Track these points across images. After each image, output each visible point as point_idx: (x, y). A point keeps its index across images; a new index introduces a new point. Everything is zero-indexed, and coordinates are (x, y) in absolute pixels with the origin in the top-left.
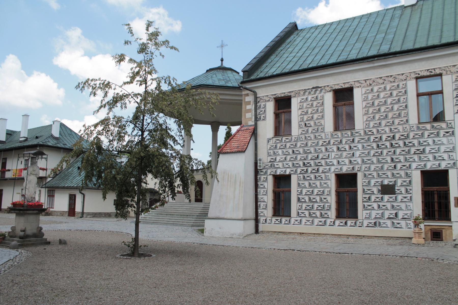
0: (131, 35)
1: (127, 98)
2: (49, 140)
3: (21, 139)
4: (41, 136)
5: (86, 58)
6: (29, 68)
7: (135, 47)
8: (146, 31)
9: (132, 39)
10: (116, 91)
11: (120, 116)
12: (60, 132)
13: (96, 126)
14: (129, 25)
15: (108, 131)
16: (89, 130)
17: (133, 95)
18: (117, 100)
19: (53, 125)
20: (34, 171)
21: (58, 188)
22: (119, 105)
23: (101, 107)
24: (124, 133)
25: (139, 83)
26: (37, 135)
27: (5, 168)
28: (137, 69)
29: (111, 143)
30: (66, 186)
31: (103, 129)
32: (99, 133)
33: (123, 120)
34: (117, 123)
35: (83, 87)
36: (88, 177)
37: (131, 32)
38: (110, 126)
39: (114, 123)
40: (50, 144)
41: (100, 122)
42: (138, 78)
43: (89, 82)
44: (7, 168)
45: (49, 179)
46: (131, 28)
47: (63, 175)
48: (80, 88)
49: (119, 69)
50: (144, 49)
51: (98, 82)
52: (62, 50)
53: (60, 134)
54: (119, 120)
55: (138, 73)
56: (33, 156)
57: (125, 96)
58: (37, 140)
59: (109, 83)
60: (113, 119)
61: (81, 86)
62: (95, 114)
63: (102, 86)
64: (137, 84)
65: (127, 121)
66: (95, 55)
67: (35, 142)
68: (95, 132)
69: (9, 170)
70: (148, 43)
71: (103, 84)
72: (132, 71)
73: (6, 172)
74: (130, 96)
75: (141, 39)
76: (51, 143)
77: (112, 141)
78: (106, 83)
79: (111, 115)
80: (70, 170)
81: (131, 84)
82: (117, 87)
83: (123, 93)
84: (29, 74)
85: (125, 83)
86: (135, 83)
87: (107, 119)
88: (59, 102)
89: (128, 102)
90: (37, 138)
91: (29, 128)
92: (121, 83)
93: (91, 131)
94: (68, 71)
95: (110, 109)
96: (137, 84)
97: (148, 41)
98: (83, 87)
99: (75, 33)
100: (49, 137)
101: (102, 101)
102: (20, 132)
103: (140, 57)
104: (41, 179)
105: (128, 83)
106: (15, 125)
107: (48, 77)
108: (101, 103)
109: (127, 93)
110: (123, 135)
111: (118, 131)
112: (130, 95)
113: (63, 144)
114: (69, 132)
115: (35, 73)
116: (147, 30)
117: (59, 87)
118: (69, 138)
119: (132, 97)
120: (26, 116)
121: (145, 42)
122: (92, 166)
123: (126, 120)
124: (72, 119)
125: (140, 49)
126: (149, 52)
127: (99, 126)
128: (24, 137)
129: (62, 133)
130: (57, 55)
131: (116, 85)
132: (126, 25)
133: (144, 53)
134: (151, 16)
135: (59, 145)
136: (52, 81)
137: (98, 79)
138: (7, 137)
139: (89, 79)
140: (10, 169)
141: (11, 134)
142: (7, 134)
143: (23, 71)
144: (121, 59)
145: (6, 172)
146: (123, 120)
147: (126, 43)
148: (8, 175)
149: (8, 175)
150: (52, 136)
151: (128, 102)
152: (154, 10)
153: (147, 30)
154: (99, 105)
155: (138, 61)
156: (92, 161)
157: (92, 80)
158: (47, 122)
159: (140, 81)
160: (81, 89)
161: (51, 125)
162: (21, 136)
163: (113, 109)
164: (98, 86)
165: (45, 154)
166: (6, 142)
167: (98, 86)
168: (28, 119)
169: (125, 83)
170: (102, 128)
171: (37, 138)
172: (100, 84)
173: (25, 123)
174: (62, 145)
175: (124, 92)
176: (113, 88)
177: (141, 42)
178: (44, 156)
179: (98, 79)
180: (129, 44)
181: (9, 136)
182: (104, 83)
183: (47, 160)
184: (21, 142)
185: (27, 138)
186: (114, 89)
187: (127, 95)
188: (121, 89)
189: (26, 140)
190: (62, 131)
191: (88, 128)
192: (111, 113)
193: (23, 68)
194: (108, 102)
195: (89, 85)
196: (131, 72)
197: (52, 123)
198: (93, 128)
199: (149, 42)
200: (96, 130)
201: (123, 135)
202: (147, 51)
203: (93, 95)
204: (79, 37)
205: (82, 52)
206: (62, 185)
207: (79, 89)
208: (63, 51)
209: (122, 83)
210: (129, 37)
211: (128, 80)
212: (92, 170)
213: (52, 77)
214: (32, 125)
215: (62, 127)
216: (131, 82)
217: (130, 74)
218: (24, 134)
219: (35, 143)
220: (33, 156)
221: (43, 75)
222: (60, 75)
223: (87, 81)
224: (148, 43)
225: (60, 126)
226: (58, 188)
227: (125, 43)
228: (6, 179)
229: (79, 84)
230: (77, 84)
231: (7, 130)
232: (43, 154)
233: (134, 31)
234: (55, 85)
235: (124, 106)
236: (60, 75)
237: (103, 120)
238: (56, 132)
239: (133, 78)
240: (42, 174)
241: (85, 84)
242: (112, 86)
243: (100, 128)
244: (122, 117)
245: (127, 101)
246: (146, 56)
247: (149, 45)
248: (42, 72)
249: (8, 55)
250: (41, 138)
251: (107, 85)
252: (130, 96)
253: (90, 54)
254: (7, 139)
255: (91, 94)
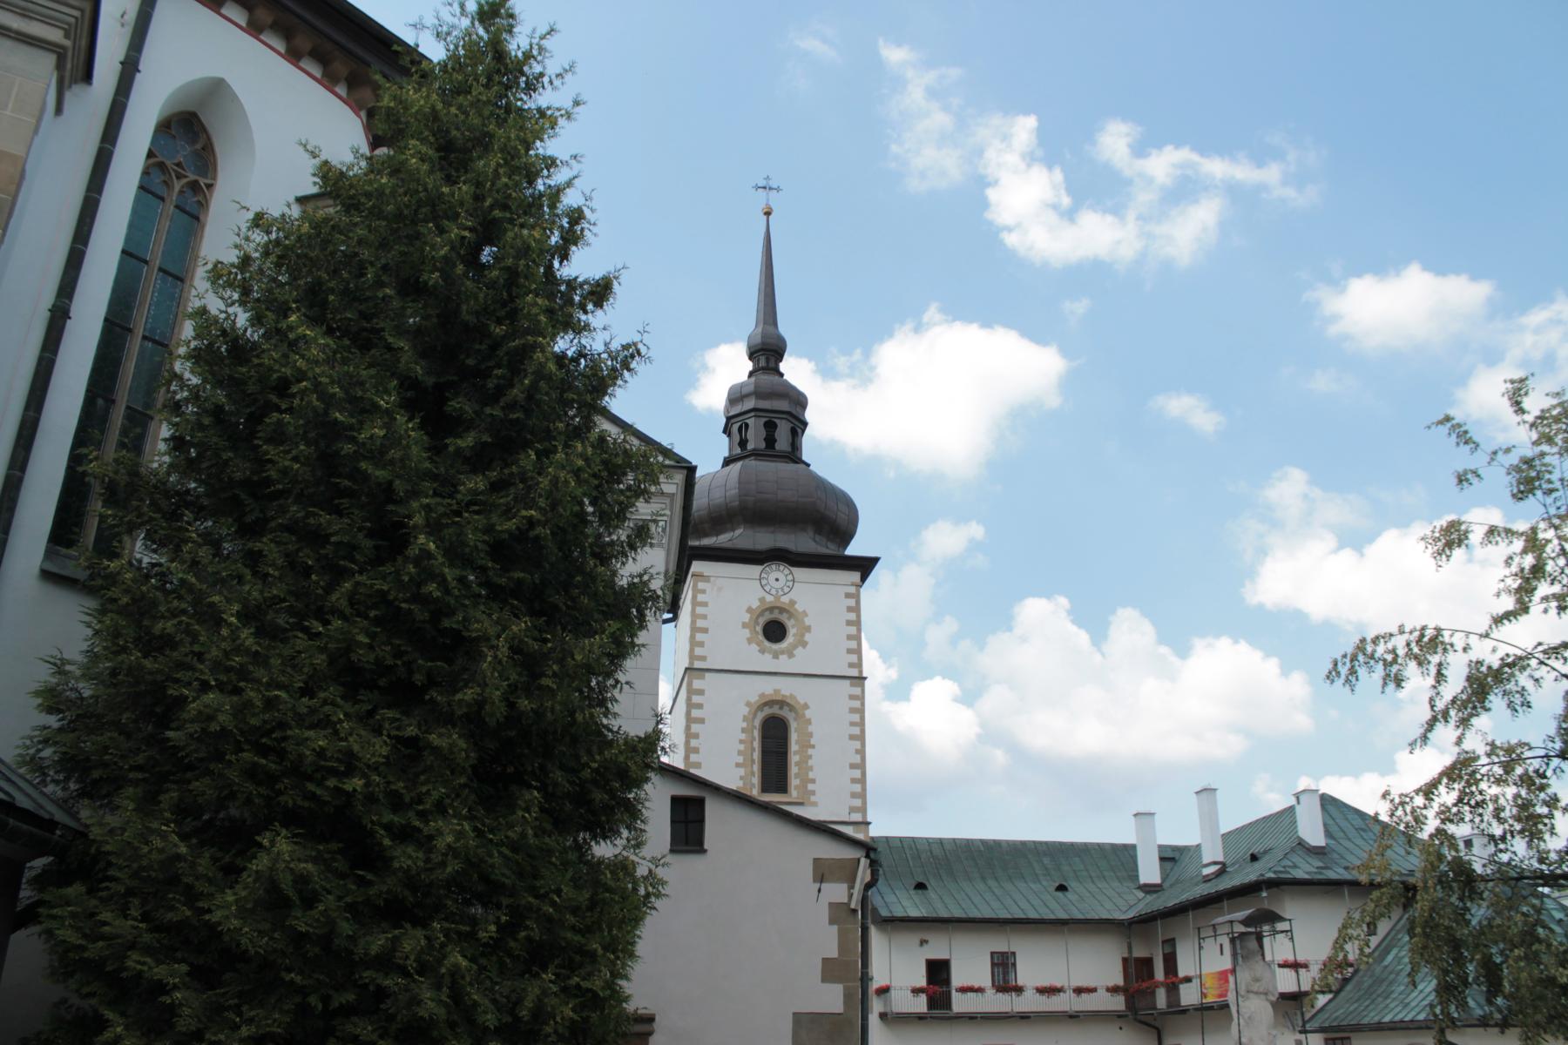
0: (1467, 447)
1: (1523, 668)
2: (1296, 859)
3: (1206, 871)
4: (1265, 852)
5: (1347, 555)
6: (1177, 637)
7: (1499, 480)
8: (1518, 418)
9: (1478, 461)
10: (1473, 655)
11: (1514, 741)
12: (1325, 825)
13: (1428, 791)
14: (1448, 419)
15: (1478, 804)
16: (1408, 809)
17: (1544, 652)
18: (1483, 685)
19: (1298, 809)
20: (1257, 980)
21: (1358, 1028)
22: (1496, 701)
23: (1431, 724)
24: (1546, 803)
25: (1554, 604)
26: (1254, 850)
27: (1175, 973)
28: (1529, 560)
29: (1502, 846)
30: (1387, 1019)
31: (1460, 800)
32: (1446, 816)
33: (1528, 754)
34: (1508, 767)
35: (1353, 671)
36: (1449, 990)
37: (1464, 437)
38: (1483, 785)
39: (1498, 770)
40: (1300, 874)
41: (1442, 774)
42: (1544, 589)
43: (1369, 649)
44: (1181, 974)
45: (1322, 1000)
46: (1459, 425)
47: (1367, 982)
48: (1343, 676)
49: (1470, 560)
50: (1532, 480)
51: (1399, 643)
52: (1262, 552)
53: (1328, 833)
54: (1510, 756)
55: (1538, 570)
56: (1242, 929)
57: (1511, 665)
58: (1257, 865)
59: (1439, 630)
60: (1489, 755)
61: (1344, 671)
62: (1417, 751)
63: (1416, 650)
64: (1546, 611)
65: (1547, 756)
66: (1371, 537)
67: (1251, 874)
68: (1430, 813)
69: (1188, 980)
70: (1543, 454)
71: (1419, 641)
72: (1514, 569)
73: (1182, 986)
74: (1533, 662)
75: (1508, 450)
76: (1304, 869)
77: (1503, 839)
78: (1429, 633)
79: (1474, 743)
80: (1390, 958)
81: (1523, 619)
82: (1473, 640)
83: (1500, 654)
84: (1183, 652)
85: (1498, 620)
86: (1536, 608)
87: (1466, 760)
88: (1303, 721)
89: (1529, 685)
90: (1254, 858)
91: (1224, 830)
92: (1483, 624)
93: (1413, 811)
94: (1299, 616)
95: (1464, 722)
96: (1546, 611)
97: (1538, 449)
98: (1353, 671)
99: (1289, 488)
100: (1293, 850)
101: (1431, 699)
102: (1198, 846)
103: (1528, 514)
104: (1292, 1001)
105: (1508, 616)
106: (1180, 830)
107: (1243, 646)
108: (1432, 707)
109: (1519, 653)
110: (1545, 810)
111: (1517, 796)
112: (1530, 656)
113: (1346, 868)
114: (1358, 822)
115: (1199, 644)
116: (1520, 410)
117: (1285, 671)
118: (1359, 842)
119: (1542, 663)
120: (1207, 792)
121: (1529, 453)
122: (1456, 945)
123: (1542, 752)
124: (1356, 773)
125: (1519, 483)
126: (1558, 485)
127: (1442, 789)
128: (1215, 863)
129: (1334, 829)
130: (1251, 573)
131: (1468, 634)
132: (1441, 422)
133: (1539, 493)
134: (1529, 339)
135: (1331, 875)
136: (1258, 655)
137: (1395, 630)
138: (1162, 867)
139: (1363, 641)
140: (1191, 973)
141: (1172, 859)
142: (1162, 859)
143: (1164, 650)
144: (1452, 538)
145: (1182, 986)
146: (1528, 754)
147: (1462, 479)
148: (1189, 996)
149: (1189, 996)
150: (1301, 844)
151: (1529, 685)
152: (1537, 317)
153: (1520, 410)
154: (1428, 715)
155: (1522, 526)
156: (1447, 928)
157: (1375, 641)
158: (1276, 802)
159: (1554, 595)
160: (1347, 681)
161: (1291, 809)
162: (1205, 861)
163: (1474, 721)
164: (1401, 652)
165: (1281, 919)
166: (1166, 885)
167: (1401, 652)
168: (1215, 802)
169: (1498, 620)
170: (1454, 796)
171: (1254, 858)
172: (1408, 645)
173: (1209, 816)
174: (1341, 871)
175: (1503, 650)
176: (1459, 647)
177: (1513, 459)
178: (1280, 926)
179: (1395, 630)
180: (1474, 480)
181: (1168, 865)
182: (1422, 636)
183: (1292, 939)
184: (1207, 879)
185: (1223, 864)
186: (1465, 650)
187: (1521, 658)
188: (1489, 644)
189: (1223, 870)
190: (1331, 822)
191: (1402, 804)
192: (1468, 734)
193: (1162, 639)
194: (1453, 701)
195: (1372, 657)
196: (1507, 572)
197: (1293, 801)
198: (1419, 801)
199: (1545, 448)
200: (1435, 805)
201: (1545, 810)
202: (1549, 482)
203: (1391, 686)
204: (1305, 496)
205: (1331, 541)
206: (1371, 1017)
207: (1340, 682)
208: (1266, 554)
209: (1487, 621)
210: (1463, 459)
211: (1508, 603)
212: (1459, 961)
213: (1254, 642)
214: (1233, 818)
215: (1330, 808)
216: (1523, 608)
217: (1509, 581)
218: (1212, 853)
219: (1253, 877)
220: (1242, 929)
221: (1224, 643)
222: (1278, 631)
223: (1361, 646)
224: (1543, 454)
225: (1323, 806)
226: (1358, 1028)
227: (1460, 481)
228: (1184, 1011)
229: (1336, 664)
230: (1330, 666)
231: (1160, 847)
232: (1273, 918)
233: (1474, 434)
234: (1272, 665)
235: (1520, 703)
236: (1278, 631)
237: (1453, 767)
238: (1312, 830)
239: (1524, 593)
240: (1286, 982)
241: (1354, 658)
242: (1455, 640)
243: (1447, 796)
244: (1522, 744)
245: (1523, 679)
246: (1549, 500)
247: (1547, 459)
248: (1218, 636)
249: (1113, 612)
250: (1267, 857)
251: (1430, 644)
252: (1533, 662)
253: (1355, 540)
254: (1164, 880)
255: (1385, 684)
